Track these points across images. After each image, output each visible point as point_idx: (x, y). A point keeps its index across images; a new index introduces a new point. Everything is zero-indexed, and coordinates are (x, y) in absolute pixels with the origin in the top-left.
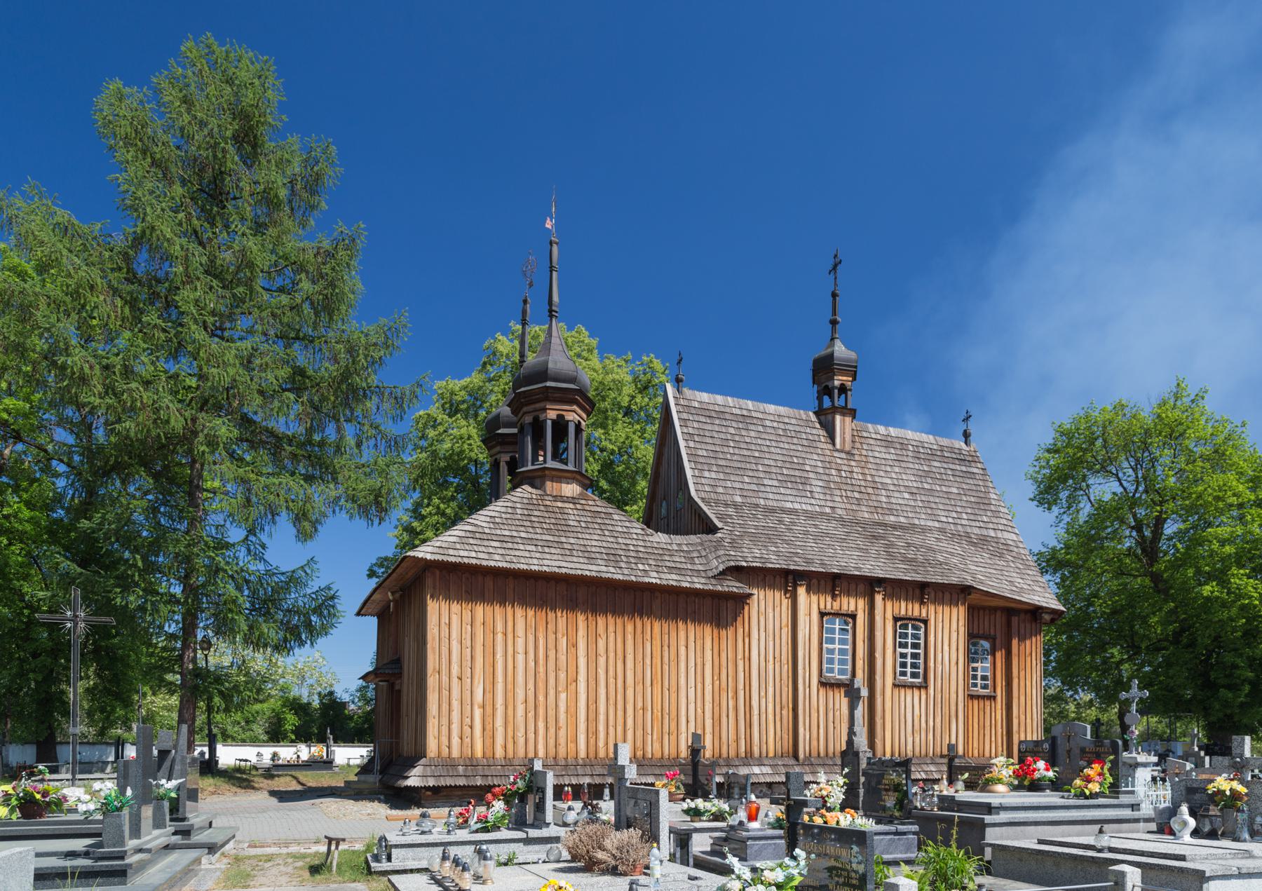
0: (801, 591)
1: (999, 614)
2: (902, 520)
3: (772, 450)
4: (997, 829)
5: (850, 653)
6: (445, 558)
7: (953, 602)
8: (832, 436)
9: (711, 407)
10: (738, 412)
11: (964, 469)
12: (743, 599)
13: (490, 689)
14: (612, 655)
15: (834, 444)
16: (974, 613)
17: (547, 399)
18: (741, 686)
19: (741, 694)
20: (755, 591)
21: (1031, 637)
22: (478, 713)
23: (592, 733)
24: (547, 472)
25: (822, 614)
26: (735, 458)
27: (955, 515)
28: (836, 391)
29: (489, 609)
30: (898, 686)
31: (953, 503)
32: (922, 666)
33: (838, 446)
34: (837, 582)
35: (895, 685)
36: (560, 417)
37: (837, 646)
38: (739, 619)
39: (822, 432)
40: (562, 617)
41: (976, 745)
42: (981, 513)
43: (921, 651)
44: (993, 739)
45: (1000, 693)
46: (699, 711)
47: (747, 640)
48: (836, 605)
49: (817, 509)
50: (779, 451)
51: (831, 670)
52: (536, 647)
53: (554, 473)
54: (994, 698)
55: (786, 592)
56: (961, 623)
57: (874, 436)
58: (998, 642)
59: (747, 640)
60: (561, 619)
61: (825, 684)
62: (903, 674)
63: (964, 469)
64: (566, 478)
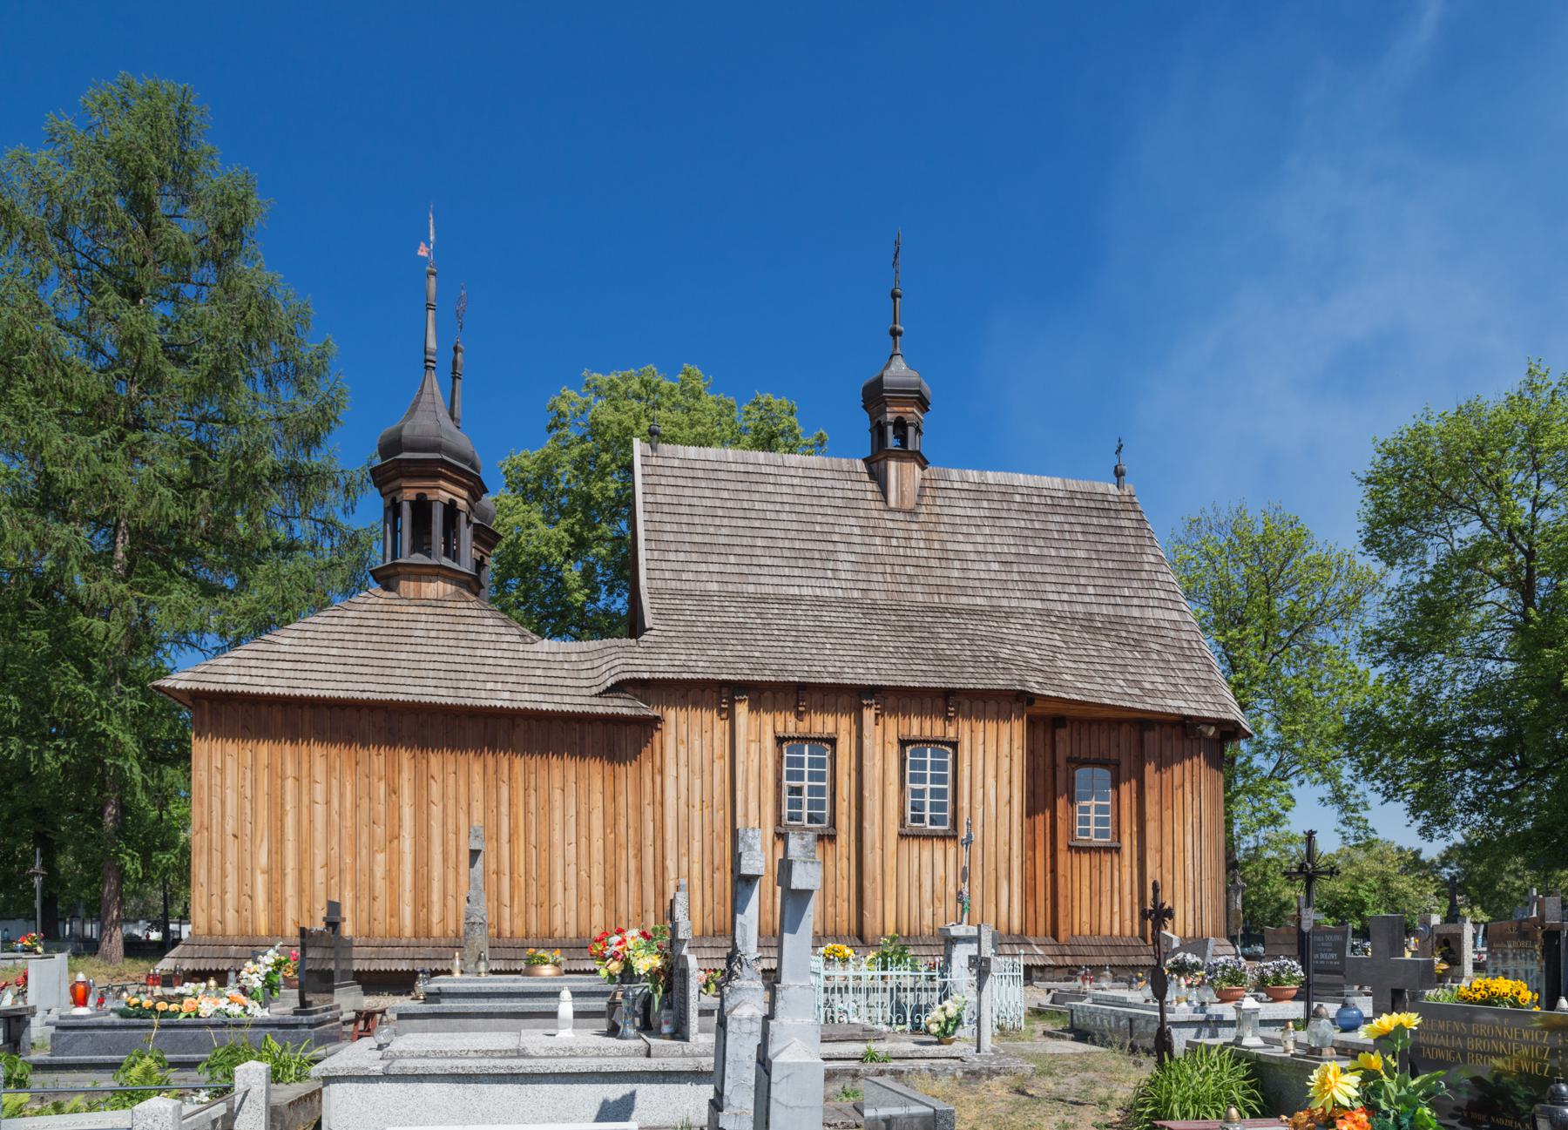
0: (742, 710)
1: (1125, 729)
2: (979, 601)
3: (784, 516)
4: (415, 1021)
5: (828, 792)
7: (1002, 716)
8: (884, 491)
9: (698, 465)
10: (742, 468)
11: (1105, 522)
12: (651, 725)
13: (277, 850)
14: (451, 803)
16: (1032, 724)
17: (403, 476)
18: (649, 840)
20: (671, 715)
21: (1191, 758)
22: (261, 880)
23: (421, 902)
24: (399, 569)
25: (780, 741)
26: (723, 531)
27: (1074, 589)
28: (890, 428)
29: (276, 748)
30: (907, 836)
31: (1074, 572)
32: (949, 807)
33: (892, 504)
34: (952, 700)
35: (902, 836)
36: (421, 497)
37: (928, 786)
38: (646, 751)
39: (874, 487)
40: (379, 754)
41: (1085, 918)
42: (1121, 583)
43: (948, 787)
44: (1116, 909)
45: (1128, 843)
46: (583, 874)
47: (658, 779)
48: (803, 727)
49: (840, 593)
50: (794, 517)
51: (1087, 832)
52: (341, 796)
53: (409, 569)
54: (1118, 850)
55: (720, 711)
56: (1017, 743)
57: (956, 485)
59: (658, 779)
60: (377, 759)
61: (1070, 848)
62: (915, 819)
63: (1105, 522)
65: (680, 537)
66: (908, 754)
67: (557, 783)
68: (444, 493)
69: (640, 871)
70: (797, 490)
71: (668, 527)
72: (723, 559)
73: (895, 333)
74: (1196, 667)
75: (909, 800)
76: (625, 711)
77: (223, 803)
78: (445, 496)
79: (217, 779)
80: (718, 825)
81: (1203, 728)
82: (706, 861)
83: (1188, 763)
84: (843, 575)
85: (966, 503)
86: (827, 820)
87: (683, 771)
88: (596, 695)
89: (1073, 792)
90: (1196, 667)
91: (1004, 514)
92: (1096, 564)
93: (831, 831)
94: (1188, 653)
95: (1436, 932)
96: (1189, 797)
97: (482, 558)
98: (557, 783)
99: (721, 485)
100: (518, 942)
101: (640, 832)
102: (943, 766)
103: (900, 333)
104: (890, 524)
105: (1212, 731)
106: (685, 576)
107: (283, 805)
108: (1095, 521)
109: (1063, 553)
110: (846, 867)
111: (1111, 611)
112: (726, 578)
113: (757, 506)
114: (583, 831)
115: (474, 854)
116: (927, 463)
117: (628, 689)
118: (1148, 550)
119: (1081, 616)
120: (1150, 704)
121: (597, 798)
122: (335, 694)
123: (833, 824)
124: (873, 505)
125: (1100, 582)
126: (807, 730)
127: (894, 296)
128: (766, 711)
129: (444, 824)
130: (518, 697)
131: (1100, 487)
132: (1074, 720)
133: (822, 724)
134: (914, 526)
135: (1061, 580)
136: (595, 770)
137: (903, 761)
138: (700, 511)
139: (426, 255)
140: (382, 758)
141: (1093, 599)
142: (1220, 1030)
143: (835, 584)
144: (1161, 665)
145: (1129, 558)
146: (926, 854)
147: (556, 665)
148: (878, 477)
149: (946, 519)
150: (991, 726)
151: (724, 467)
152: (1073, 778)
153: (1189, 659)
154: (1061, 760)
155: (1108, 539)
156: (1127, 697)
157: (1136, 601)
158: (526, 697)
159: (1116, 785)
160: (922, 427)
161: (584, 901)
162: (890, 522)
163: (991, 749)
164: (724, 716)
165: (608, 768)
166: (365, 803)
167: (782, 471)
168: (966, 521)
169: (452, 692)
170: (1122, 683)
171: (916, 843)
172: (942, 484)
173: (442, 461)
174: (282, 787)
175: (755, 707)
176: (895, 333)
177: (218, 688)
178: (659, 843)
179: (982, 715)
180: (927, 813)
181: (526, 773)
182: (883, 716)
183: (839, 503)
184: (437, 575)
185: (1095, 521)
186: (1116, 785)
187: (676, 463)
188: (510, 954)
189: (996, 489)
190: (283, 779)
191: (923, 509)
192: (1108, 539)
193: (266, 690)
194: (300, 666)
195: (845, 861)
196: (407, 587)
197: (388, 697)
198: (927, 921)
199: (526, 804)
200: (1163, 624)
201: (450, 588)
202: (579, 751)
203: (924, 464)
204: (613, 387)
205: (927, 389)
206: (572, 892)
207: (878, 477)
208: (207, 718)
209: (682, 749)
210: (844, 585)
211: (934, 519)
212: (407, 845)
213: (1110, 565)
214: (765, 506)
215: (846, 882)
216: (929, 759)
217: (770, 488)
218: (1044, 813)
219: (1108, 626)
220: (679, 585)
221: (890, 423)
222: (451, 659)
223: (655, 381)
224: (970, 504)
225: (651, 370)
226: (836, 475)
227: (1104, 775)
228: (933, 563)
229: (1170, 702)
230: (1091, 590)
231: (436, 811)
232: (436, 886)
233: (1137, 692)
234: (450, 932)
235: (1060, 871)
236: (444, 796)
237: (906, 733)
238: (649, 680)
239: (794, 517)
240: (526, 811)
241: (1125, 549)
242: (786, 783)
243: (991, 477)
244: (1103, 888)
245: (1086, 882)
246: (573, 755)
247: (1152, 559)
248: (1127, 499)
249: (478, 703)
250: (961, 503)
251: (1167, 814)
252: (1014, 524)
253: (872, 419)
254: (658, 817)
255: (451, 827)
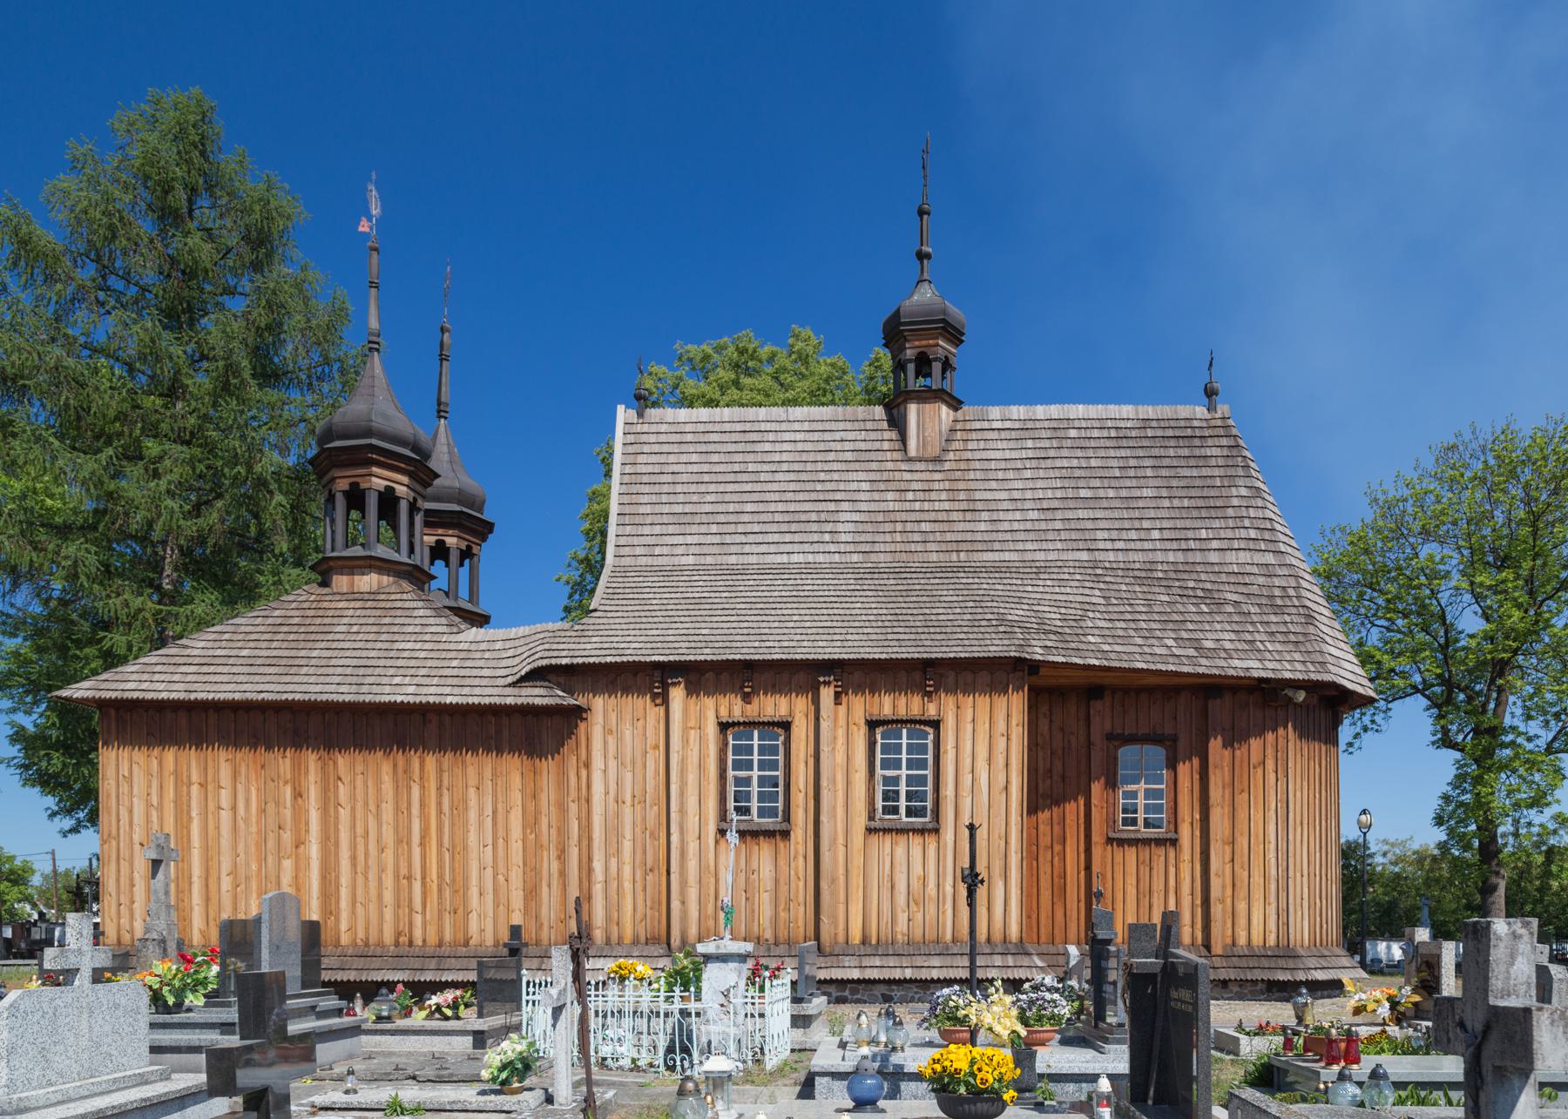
0: (677, 694)
2: (1007, 556)
5: (781, 783)
6: (361, 698)
8: (903, 439)
9: (688, 428)
10: (739, 427)
12: (576, 714)
14: (359, 805)
15: (905, 450)
19: (574, 853)
21: (1274, 730)
24: (331, 563)
25: (724, 727)
32: (930, 797)
33: (912, 452)
35: (870, 831)
36: (354, 486)
39: (894, 435)
42: (1198, 524)
49: (837, 558)
50: (792, 476)
52: (248, 801)
53: (340, 563)
54: (1174, 842)
55: (654, 696)
58: (1182, 744)
59: (584, 773)
60: (283, 762)
64: (361, 567)
65: (658, 509)
66: (879, 737)
67: (472, 781)
68: (378, 479)
69: (563, 874)
70: (800, 446)
71: (645, 499)
72: (703, 529)
73: (922, 256)
74: (1288, 619)
75: (880, 789)
76: (538, 701)
77: (131, 812)
78: (379, 484)
79: (125, 788)
80: (651, 822)
81: (1289, 692)
82: (637, 862)
83: (1270, 736)
84: (843, 538)
85: (1005, 445)
86: (780, 813)
87: (612, 764)
88: (509, 685)
89: (1115, 774)
90: (1288, 619)
91: (1052, 453)
92: (1166, 503)
93: (784, 826)
94: (1279, 602)
95: (1421, 951)
96: (1271, 777)
97: (469, 548)
98: (472, 781)
99: (711, 448)
100: (429, 951)
101: (563, 832)
102: (923, 749)
103: (928, 256)
104: (907, 476)
105: (1301, 696)
106: (657, 551)
107: (189, 812)
108: (1171, 452)
109: (1124, 493)
110: (801, 867)
111: (1180, 557)
112: (705, 550)
113: (751, 467)
114: (501, 833)
115: (156, 864)
116: (961, 403)
117: (551, 677)
118: (1241, 482)
119: (1137, 566)
120: (1205, 667)
121: (516, 797)
122: (230, 696)
123: (787, 818)
124: (889, 456)
125: (1166, 524)
126: (756, 714)
127: (921, 213)
128: (708, 694)
129: (353, 827)
130: (425, 690)
131: (1184, 411)
132: (1114, 690)
133: (772, 706)
134: (937, 476)
135: (1117, 525)
136: (513, 767)
137: (871, 745)
138: (684, 478)
139: (366, 229)
140: (288, 761)
141: (1158, 545)
142: (904, 1085)
143: (832, 548)
144: (1236, 618)
145: (1212, 493)
146: (900, 851)
147: (478, 655)
148: (897, 422)
149: (978, 465)
150: (983, 701)
151: (717, 427)
152: (1116, 758)
153: (1279, 610)
154: (1097, 737)
155: (1187, 472)
156: (1171, 660)
157: (1215, 544)
158: (433, 690)
159: (1172, 765)
160: (954, 361)
161: (501, 907)
162: (916, 477)
163: (983, 728)
164: (658, 701)
165: (527, 762)
166: (271, 807)
167: (784, 426)
168: (1003, 465)
169: (354, 689)
170: (1170, 643)
171: (888, 838)
172: (978, 425)
173: (371, 446)
174: (189, 793)
175: (693, 690)
176: (922, 256)
177: (113, 695)
178: (585, 843)
179: (969, 689)
180: (903, 803)
181: (440, 771)
182: (847, 694)
183: (849, 456)
184: (370, 567)
185: (1171, 452)
186: (1172, 765)
187: (664, 428)
188: (417, 963)
189: (1046, 424)
190: (190, 784)
191: (951, 456)
192: (1187, 472)
193: (164, 695)
194: (205, 669)
195: (801, 859)
196: (341, 582)
197: (284, 697)
198: (902, 926)
199: (439, 804)
200: (1249, 569)
201: (385, 579)
202: (496, 745)
203: (955, 404)
204: (706, 358)
205: (956, 313)
206: (490, 897)
207: (897, 422)
208: (113, 726)
209: (611, 740)
210: (842, 548)
211: (963, 465)
212: (314, 850)
213: (1186, 503)
214: (759, 467)
215: (801, 884)
216: (904, 741)
217: (768, 447)
218: (1076, 800)
219: (1173, 575)
220: (649, 561)
221: (910, 361)
222: (365, 654)
223: (751, 347)
224: (1012, 444)
225: (748, 338)
226: (849, 426)
227: (1157, 753)
228: (955, 516)
229: (1236, 663)
230: (1156, 534)
231: (344, 814)
232: (344, 893)
233: (1192, 652)
234: (359, 941)
235: (1096, 868)
236: (353, 798)
237: (876, 712)
238: (567, 665)
239: (792, 476)
240: (440, 812)
241: (1209, 482)
242: (731, 773)
243: (1040, 411)
244: (1155, 888)
245: (1131, 880)
246: (488, 750)
247: (1244, 492)
248: (1219, 423)
249: (378, 699)
250: (1000, 445)
251: (1241, 799)
252: (1065, 463)
253: (893, 358)
254: (584, 815)
255: (360, 830)
